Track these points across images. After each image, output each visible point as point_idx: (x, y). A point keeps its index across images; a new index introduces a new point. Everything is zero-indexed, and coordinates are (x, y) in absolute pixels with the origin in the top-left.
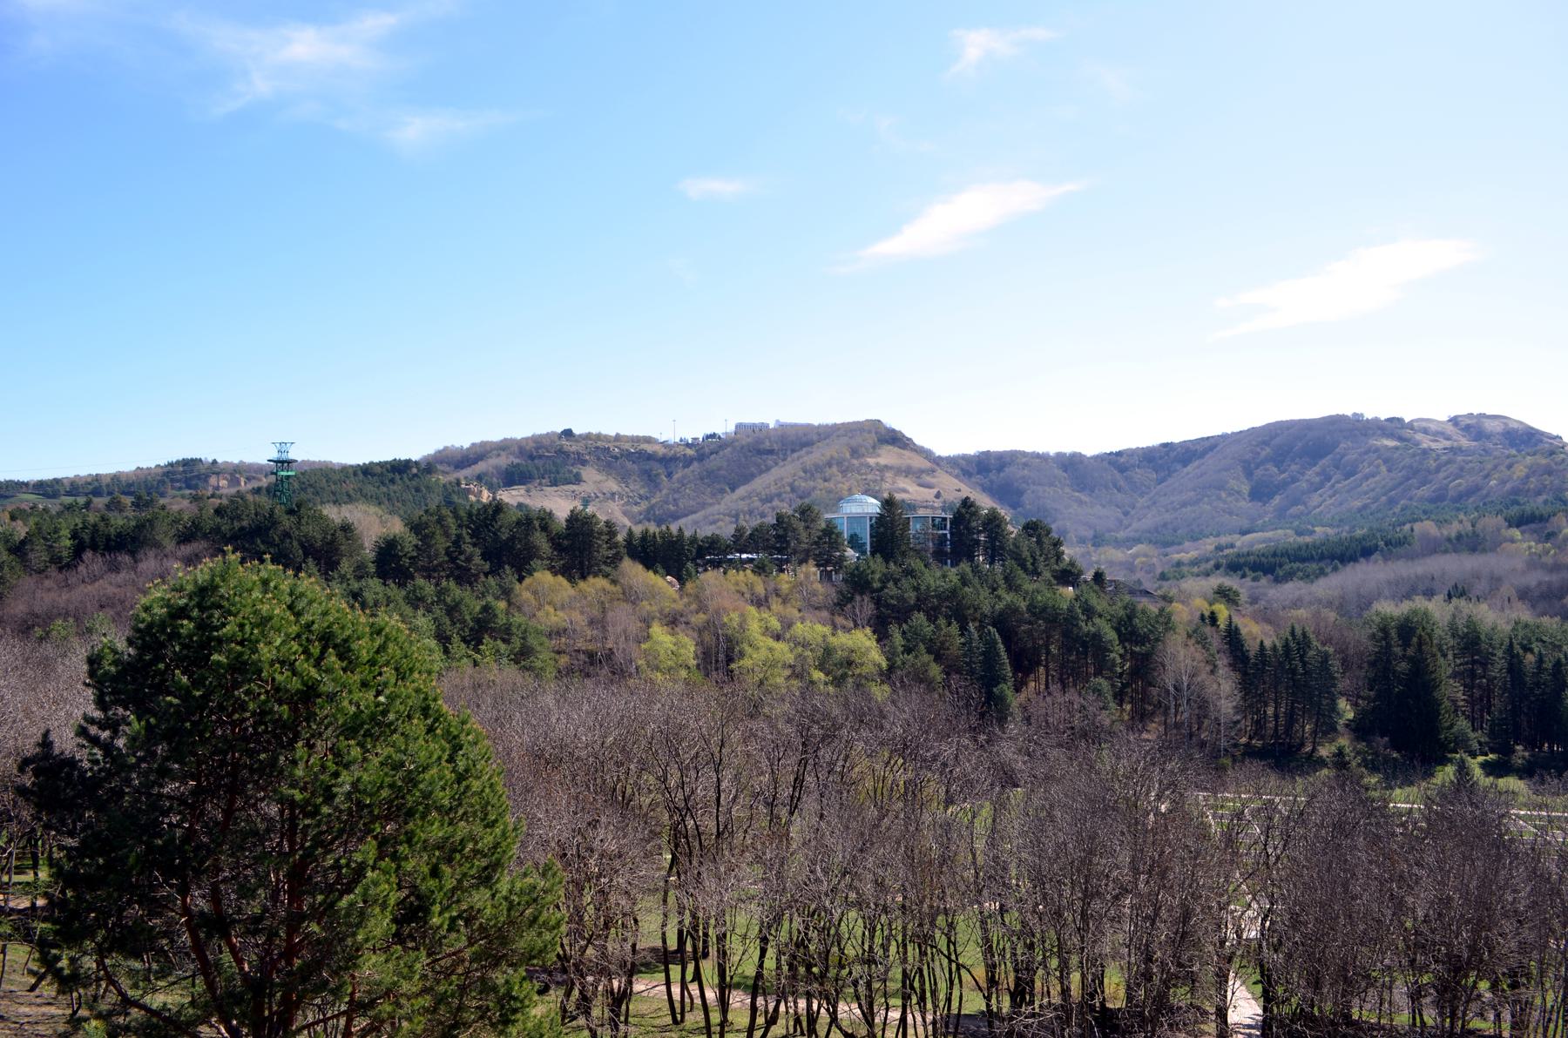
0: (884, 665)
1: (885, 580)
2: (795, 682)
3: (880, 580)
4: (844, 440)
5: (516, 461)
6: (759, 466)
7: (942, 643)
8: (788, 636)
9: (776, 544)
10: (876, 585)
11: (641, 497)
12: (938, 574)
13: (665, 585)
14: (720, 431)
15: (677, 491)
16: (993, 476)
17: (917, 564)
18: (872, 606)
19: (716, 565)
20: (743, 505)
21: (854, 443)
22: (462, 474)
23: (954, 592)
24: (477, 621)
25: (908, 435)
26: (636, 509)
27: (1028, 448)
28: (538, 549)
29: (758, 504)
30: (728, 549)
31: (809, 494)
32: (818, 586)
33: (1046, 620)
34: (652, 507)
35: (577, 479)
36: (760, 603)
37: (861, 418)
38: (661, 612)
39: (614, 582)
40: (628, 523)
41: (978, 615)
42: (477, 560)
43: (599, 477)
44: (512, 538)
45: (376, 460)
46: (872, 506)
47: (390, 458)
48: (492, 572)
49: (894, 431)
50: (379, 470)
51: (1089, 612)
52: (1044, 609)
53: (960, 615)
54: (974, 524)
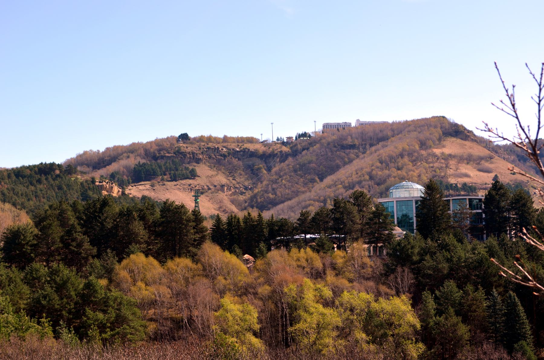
0: (418, 326)
1: (424, 252)
2: (342, 342)
3: (419, 254)
5: (143, 161)
6: (342, 158)
7: (470, 306)
8: (337, 303)
9: (334, 225)
10: (415, 258)
11: (246, 188)
12: (469, 247)
13: (237, 264)
14: (310, 129)
15: (275, 182)
17: (450, 239)
18: (411, 276)
19: (287, 245)
20: (330, 193)
21: (422, 137)
22: (97, 175)
23: (480, 263)
24: (82, 296)
26: (241, 198)
28: (137, 235)
31: (385, 181)
32: (367, 260)
34: (255, 196)
35: (193, 175)
36: (318, 275)
37: (428, 115)
39: (196, 261)
42: (87, 245)
44: (116, 227)
45: (27, 164)
46: (417, 190)
47: (37, 163)
48: (98, 256)
49: (456, 125)
50: (28, 172)
53: (486, 279)
54: (503, 204)
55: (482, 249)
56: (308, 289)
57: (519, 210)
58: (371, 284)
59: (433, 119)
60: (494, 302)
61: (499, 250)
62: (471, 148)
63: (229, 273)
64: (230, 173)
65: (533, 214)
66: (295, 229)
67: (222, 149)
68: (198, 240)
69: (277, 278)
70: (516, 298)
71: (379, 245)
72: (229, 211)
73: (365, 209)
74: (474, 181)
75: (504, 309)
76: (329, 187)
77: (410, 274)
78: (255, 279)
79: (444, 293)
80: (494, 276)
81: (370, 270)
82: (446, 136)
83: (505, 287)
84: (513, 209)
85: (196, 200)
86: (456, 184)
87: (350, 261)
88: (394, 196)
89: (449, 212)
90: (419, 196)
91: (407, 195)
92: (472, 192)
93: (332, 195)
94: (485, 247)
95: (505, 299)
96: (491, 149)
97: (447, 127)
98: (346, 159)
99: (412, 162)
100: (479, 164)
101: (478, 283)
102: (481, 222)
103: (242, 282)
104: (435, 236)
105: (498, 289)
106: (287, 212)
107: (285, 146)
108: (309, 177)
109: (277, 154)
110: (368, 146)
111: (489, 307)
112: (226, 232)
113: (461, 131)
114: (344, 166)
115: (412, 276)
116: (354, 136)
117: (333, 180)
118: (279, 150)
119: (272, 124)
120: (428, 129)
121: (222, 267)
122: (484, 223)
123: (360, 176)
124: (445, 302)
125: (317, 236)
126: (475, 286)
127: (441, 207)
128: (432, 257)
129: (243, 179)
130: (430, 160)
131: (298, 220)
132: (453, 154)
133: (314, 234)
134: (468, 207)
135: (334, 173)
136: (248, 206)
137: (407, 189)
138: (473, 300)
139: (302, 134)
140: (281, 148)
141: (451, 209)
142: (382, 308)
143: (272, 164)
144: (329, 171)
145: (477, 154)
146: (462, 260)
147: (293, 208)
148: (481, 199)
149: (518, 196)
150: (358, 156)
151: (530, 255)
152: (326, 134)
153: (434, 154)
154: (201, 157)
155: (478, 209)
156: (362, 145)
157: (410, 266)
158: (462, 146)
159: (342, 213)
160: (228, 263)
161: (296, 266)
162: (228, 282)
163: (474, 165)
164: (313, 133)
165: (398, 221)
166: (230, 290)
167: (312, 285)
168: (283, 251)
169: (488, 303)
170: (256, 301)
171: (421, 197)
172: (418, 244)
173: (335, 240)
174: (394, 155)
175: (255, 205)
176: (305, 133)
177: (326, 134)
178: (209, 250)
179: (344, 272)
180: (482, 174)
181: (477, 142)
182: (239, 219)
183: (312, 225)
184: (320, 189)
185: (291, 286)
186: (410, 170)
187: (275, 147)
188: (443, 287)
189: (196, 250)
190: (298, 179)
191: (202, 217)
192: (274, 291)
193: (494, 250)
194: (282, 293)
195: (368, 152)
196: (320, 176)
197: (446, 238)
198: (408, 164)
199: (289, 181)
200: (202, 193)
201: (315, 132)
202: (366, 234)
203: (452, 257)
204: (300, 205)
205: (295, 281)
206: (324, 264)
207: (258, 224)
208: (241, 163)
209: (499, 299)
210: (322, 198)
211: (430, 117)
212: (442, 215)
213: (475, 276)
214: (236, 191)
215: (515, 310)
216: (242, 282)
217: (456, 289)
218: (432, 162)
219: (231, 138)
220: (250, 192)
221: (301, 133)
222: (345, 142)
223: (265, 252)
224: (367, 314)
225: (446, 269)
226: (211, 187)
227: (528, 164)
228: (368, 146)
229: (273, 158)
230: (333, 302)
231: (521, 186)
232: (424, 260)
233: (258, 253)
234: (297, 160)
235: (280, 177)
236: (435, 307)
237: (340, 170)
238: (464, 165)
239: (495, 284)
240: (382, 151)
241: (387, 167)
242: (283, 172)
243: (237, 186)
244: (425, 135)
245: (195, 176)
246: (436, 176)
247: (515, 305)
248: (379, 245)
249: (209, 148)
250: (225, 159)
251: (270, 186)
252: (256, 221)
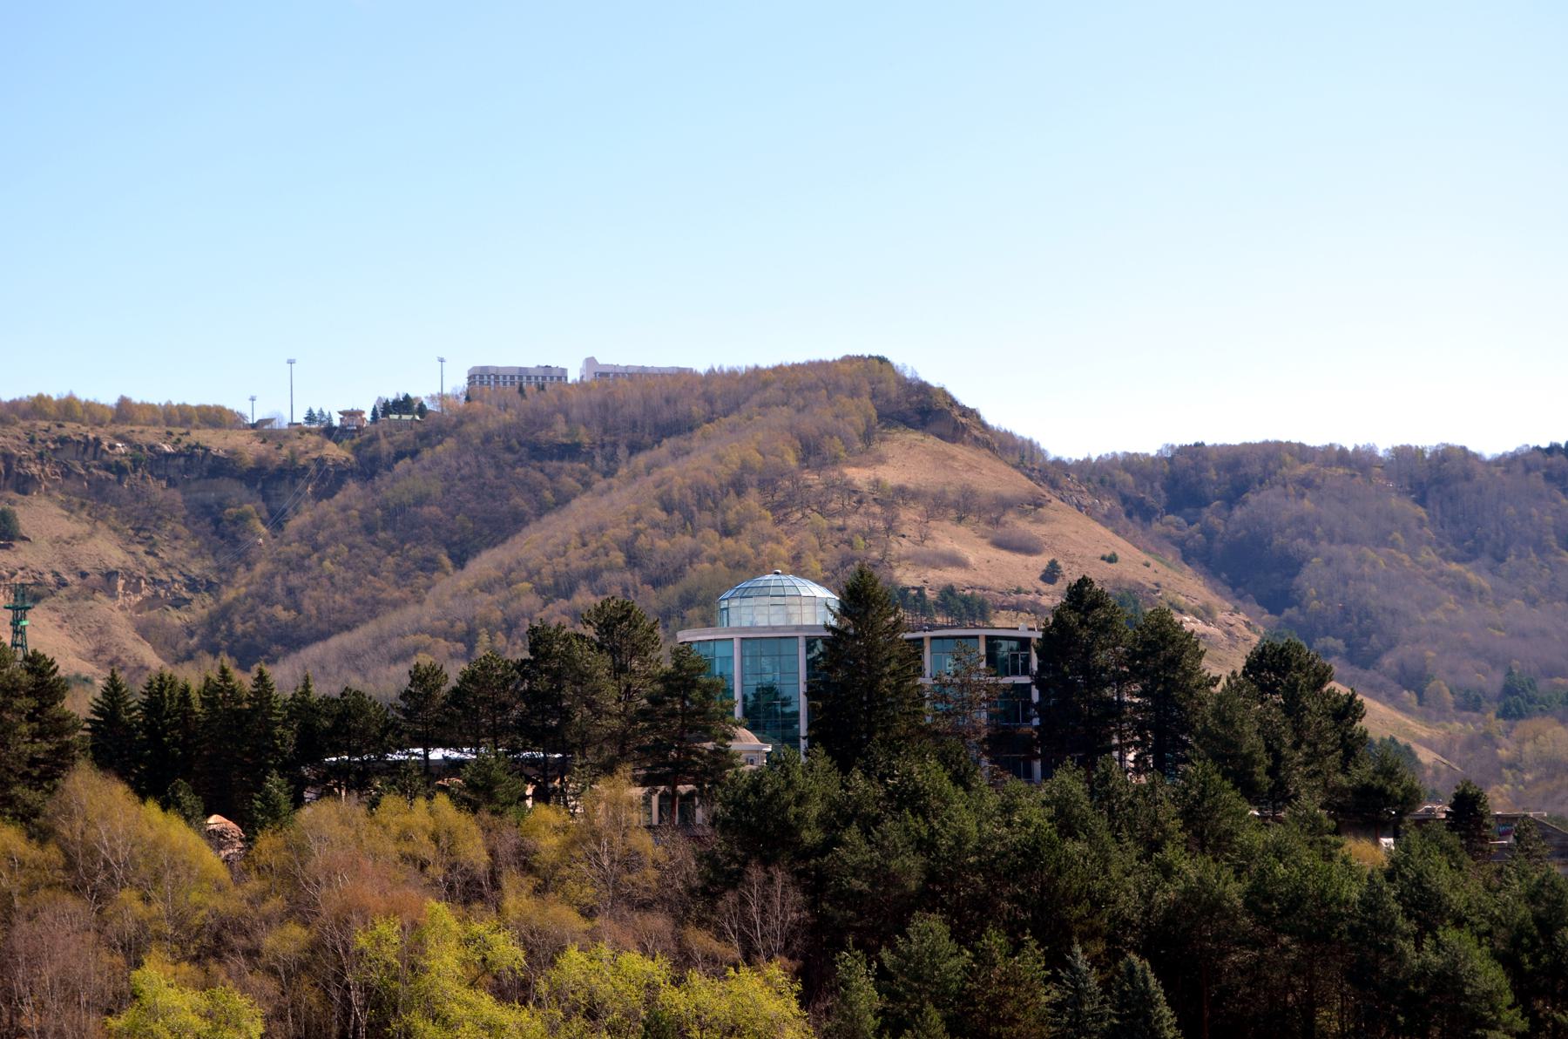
1: (840, 816)
3: (822, 821)
4: (781, 415)
6: (534, 491)
7: (995, 1003)
8: (543, 988)
9: (524, 717)
11: (193, 585)
12: (992, 801)
13: (190, 848)
14: (423, 390)
15: (297, 565)
17: (929, 773)
19: (358, 779)
20: (487, 606)
21: (808, 424)
23: (1031, 855)
26: (176, 618)
27: (1315, 437)
29: (531, 601)
30: (393, 732)
31: (679, 572)
33: (1307, 938)
34: (224, 613)
36: (471, 891)
37: (831, 352)
38: (180, 922)
39: (42, 836)
40: (153, 660)
41: (1103, 922)
43: (68, 526)
46: (812, 604)
49: (924, 388)
51: (1427, 909)
52: (1296, 901)
54: (1102, 657)
56: (441, 940)
57: (1155, 681)
58: (659, 922)
59: (846, 367)
60: (1077, 990)
61: (1090, 813)
62: (971, 467)
63: (157, 878)
64: (138, 530)
66: (390, 726)
67: (112, 447)
68: (43, 761)
69: (329, 900)
70: (1150, 976)
71: (683, 789)
72: (131, 664)
73: (635, 663)
74: (980, 581)
75: (1110, 1015)
76: (487, 588)
79: (908, 958)
80: (1077, 901)
81: (653, 874)
82: (889, 426)
83: (1111, 939)
84: (1136, 674)
85: (15, 623)
86: (920, 590)
89: (920, 681)
90: (820, 622)
91: (777, 620)
92: (974, 616)
93: (497, 615)
94: (1045, 804)
95: (1112, 979)
96: (1035, 474)
97: (893, 395)
98: (548, 495)
99: (773, 509)
100: (996, 522)
102: (1028, 719)
103: (204, 912)
105: (1088, 945)
106: (353, 664)
107: (336, 441)
108: (416, 552)
109: (305, 468)
110: (622, 452)
111: (1058, 1007)
112: (141, 735)
113: (941, 410)
114: (539, 516)
115: (800, 898)
116: (575, 413)
117: (500, 566)
118: (315, 455)
119: (291, 362)
121: (132, 858)
123: (594, 554)
124: (910, 989)
125: (467, 754)
126: (1011, 933)
127: (894, 665)
129: (181, 554)
130: (833, 505)
131: (403, 697)
132: (911, 486)
133: (456, 746)
134: (983, 665)
135: (503, 541)
136: (200, 646)
137: (777, 600)
140: (318, 447)
141: (927, 673)
142: (697, 1006)
143: (287, 502)
144: (486, 531)
147: (358, 656)
148: (1029, 639)
149: (1152, 632)
150: (587, 485)
152: (478, 404)
153: (849, 483)
154: (35, 469)
155: (1015, 673)
156: (603, 446)
158: (943, 460)
159: (557, 676)
160: (155, 845)
162: (154, 909)
163: (982, 525)
164: (432, 398)
165: (744, 706)
166: (160, 937)
167: (455, 927)
168: (348, 805)
169: (1055, 993)
170: (255, 980)
172: (819, 789)
173: (530, 771)
174: (714, 483)
175: (225, 644)
176: (407, 398)
178: (85, 795)
179: (562, 881)
180: (1005, 556)
181: (993, 450)
182: (186, 690)
183: (452, 716)
184: (454, 596)
185: (382, 928)
186: (767, 538)
187: (300, 445)
188: (905, 935)
189: (38, 796)
190: (379, 559)
191: (60, 679)
192: (315, 947)
193: (1076, 812)
194: (346, 952)
195: (623, 471)
196: (456, 551)
197: (916, 769)
198: (760, 518)
199: (347, 565)
200: (37, 599)
201: (442, 397)
202: (638, 749)
203: (933, 833)
204: (382, 650)
207: (255, 710)
208: (176, 496)
209: (1093, 981)
210: (461, 626)
211: (838, 356)
213: (1015, 898)
214: (156, 595)
215: (1148, 1018)
216: (204, 912)
217: (952, 947)
219: (144, 407)
220: (209, 601)
221: (391, 397)
222: (543, 436)
223: (285, 807)
224: (647, 1027)
225: (915, 874)
227: (1157, 527)
228: (622, 452)
229: (293, 483)
230: (525, 985)
231: (1136, 602)
232: (841, 843)
233: (260, 811)
234: (375, 491)
235: (316, 548)
236: (878, 1005)
237: (525, 530)
238: (947, 523)
239: (1077, 928)
240: (670, 469)
241: (689, 522)
243: (163, 576)
245: (12, 538)
247: (1147, 1000)
248: (683, 789)
249: (63, 441)
250: (120, 482)
251: (278, 579)
252: (249, 699)
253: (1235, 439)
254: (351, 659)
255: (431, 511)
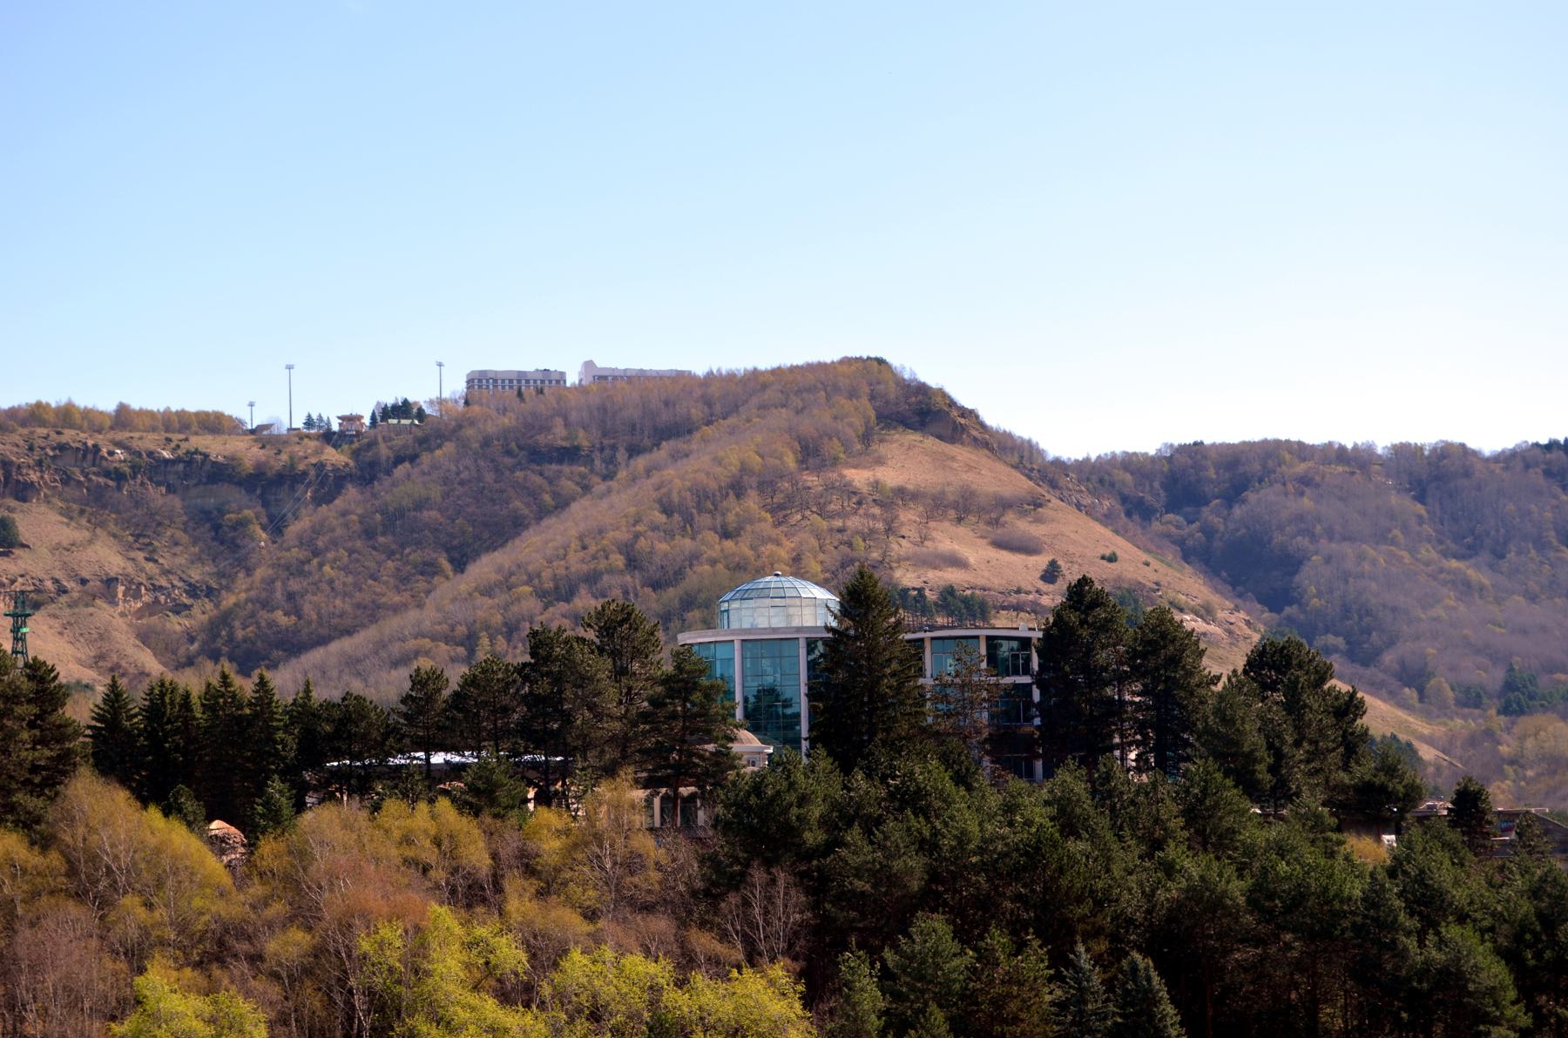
1: (842, 817)
3: (824, 822)
4: (781, 417)
6: (534, 494)
7: (999, 1003)
8: (546, 991)
9: (527, 720)
10: (813, 837)
11: (193, 591)
12: (994, 801)
13: (191, 853)
14: (422, 393)
15: (297, 570)
16: (1210, 514)
17: (929, 773)
19: (359, 785)
20: (488, 610)
21: (807, 425)
25: (964, 399)
26: (177, 624)
29: (531, 605)
30: (393, 737)
31: (679, 574)
32: (646, 844)
34: (225, 619)
36: (473, 894)
37: (830, 355)
38: (183, 927)
39: (44, 843)
40: (153, 666)
43: (67, 533)
46: (812, 605)
49: (923, 389)
51: (1429, 906)
52: (1298, 899)
54: (1102, 657)
55: (1036, 806)
56: (444, 943)
58: (661, 924)
59: (845, 368)
60: (1081, 990)
61: (1092, 812)
63: (160, 884)
64: (138, 536)
65: (1203, 692)
66: (391, 731)
67: (111, 453)
68: (44, 768)
69: (332, 904)
70: (1154, 974)
71: (685, 791)
72: (132, 670)
73: (636, 666)
74: (981, 582)
75: (1114, 1014)
76: (488, 592)
77: (793, 892)
78: (253, 907)
79: (912, 958)
80: (1079, 900)
81: (655, 876)
82: (888, 427)
83: (1114, 938)
84: (1137, 673)
85: (15, 630)
86: (920, 590)
87: (586, 844)
88: (735, 625)
89: (921, 681)
90: (820, 623)
91: (778, 622)
94: (1047, 803)
95: (1115, 977)
97: (892, 396)
98: (547, 498)
99: (772, 511)
100: (995, 523)
101: (1025, 926)
102: (1029, 719)
103: (207, 917)
104: (877, 762)
105: (1091, 943)
106: (357, 668)
107: (335, 446)
108: (416, 556)
109: (305, 474)
110: (621, 455)
111: (1062, 1006)
114: (539, 519)
116: (574, 416)
117: (499, 570)
118: (314, 460)
119: (289, 367)
120: (828, 398)
121: (135, 864)
122: (1037, 721)
123: (594, 557)
125: (469, 758)
126: (1014, 933)
127: (895, 665)
128: (871, 833)
129: (181, 560)
130: (832, 507)
131: (404, 701)
132: (910, 487)
134: (984, 665)
135: (502, 545)
137: (777, 602)
138: (1008, 981)
139: (395, 408)
140: (318, 452)
141: (928, 673)
142: (700, 1008)
143: (287, 508)
144: (486, 535)
145: (992, 489)
146: (971, 846)
147: (359, 661)
150: (586, 489)
151: (1197, 832)
153: (849, 484)
154: (34, 476)
155: (1016, 673)
156: (602, 450)
157: (793, 863)
158: (943, 461)
159: (558, 679)
160: (158, 851)
161: (398, 861)
162: (157, 914)
163: (982, 525)
164: (431, 402)
165: (745, 708)
166: (163, 943)
167: (458, 930)
168: (350, 808)
169: (1059, 992)
171: (828, 629)
172: (821, 790)
173: (531, 774)
174: (713, 485)
175: (225, 649)
176: (406, 402)
177: (476, 408)
179: (565, 884)
180: (1005, 556)
181: (992, 450)
182: (187, 696)
183: (453, 719)
184: (454, 600)
185: (386, 932)
187: (299, 451)
189: (40, 802)
190: (379, 564)
191: (61, 686)
192: (318, 952)
193: (1078, 811)
194: (349, 956)
195: (622, 474)
197: (917, 770)
198: (760, 520)
199: (346, 569)
200: (37, 606)
203: (936, 833)
204: (384, 654)
205: (395, 916)
206: (495, 856)
207: (256, 715)
208: (176, 502)
209: (1096, 980)
210: (462, 630)
211: (836, 357)
212: (898, 690)
213: (1018, 898)
215: (1151, 1016)
216: (207, 917)
218: (842, 514)
219: (142, 413)
220: (209, 606)
221: (390, 401)
222: (542, 439)
225: (918, 874)
226: (69, 585)
228: (621, 455)
229: (292, 488)
230: (528, 988)
231: (1136, 601)
232: (842, 844)
233: (262, 816)
234: (374, 496)
235: (316, 553)
236: (882, 1005)
237: (525, 534)
238: (947, 524)
239: (1080, 927)
240: (669, 472)
242: (327, 538)
243: (163, 582)
244: (818, 418)
245: (12, 545)
246: (852, 561)
247: (1150, 999)
248: (685, 791)
249: (62, 448)
250: (119, 488)
251: (278, 584)
252: (250, 704)
253: (1235, 439)
254: (352, 663)
255: (430, 515)
